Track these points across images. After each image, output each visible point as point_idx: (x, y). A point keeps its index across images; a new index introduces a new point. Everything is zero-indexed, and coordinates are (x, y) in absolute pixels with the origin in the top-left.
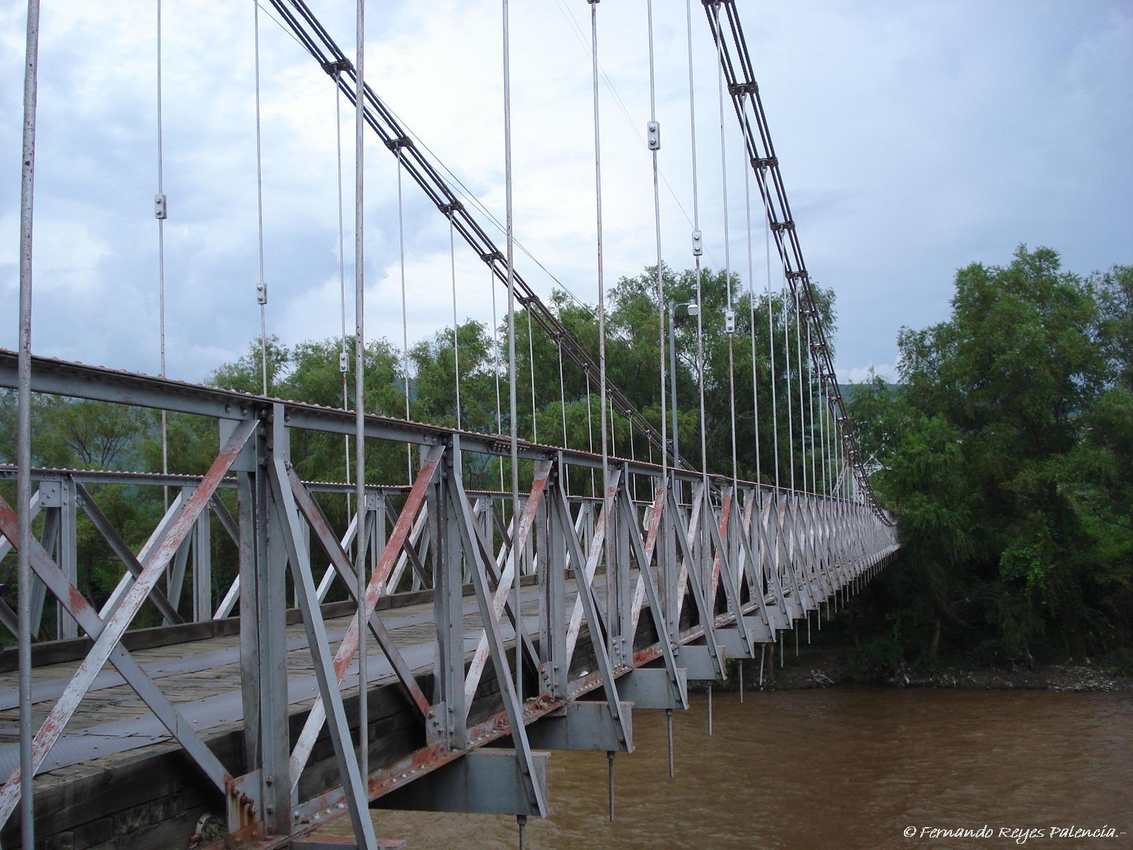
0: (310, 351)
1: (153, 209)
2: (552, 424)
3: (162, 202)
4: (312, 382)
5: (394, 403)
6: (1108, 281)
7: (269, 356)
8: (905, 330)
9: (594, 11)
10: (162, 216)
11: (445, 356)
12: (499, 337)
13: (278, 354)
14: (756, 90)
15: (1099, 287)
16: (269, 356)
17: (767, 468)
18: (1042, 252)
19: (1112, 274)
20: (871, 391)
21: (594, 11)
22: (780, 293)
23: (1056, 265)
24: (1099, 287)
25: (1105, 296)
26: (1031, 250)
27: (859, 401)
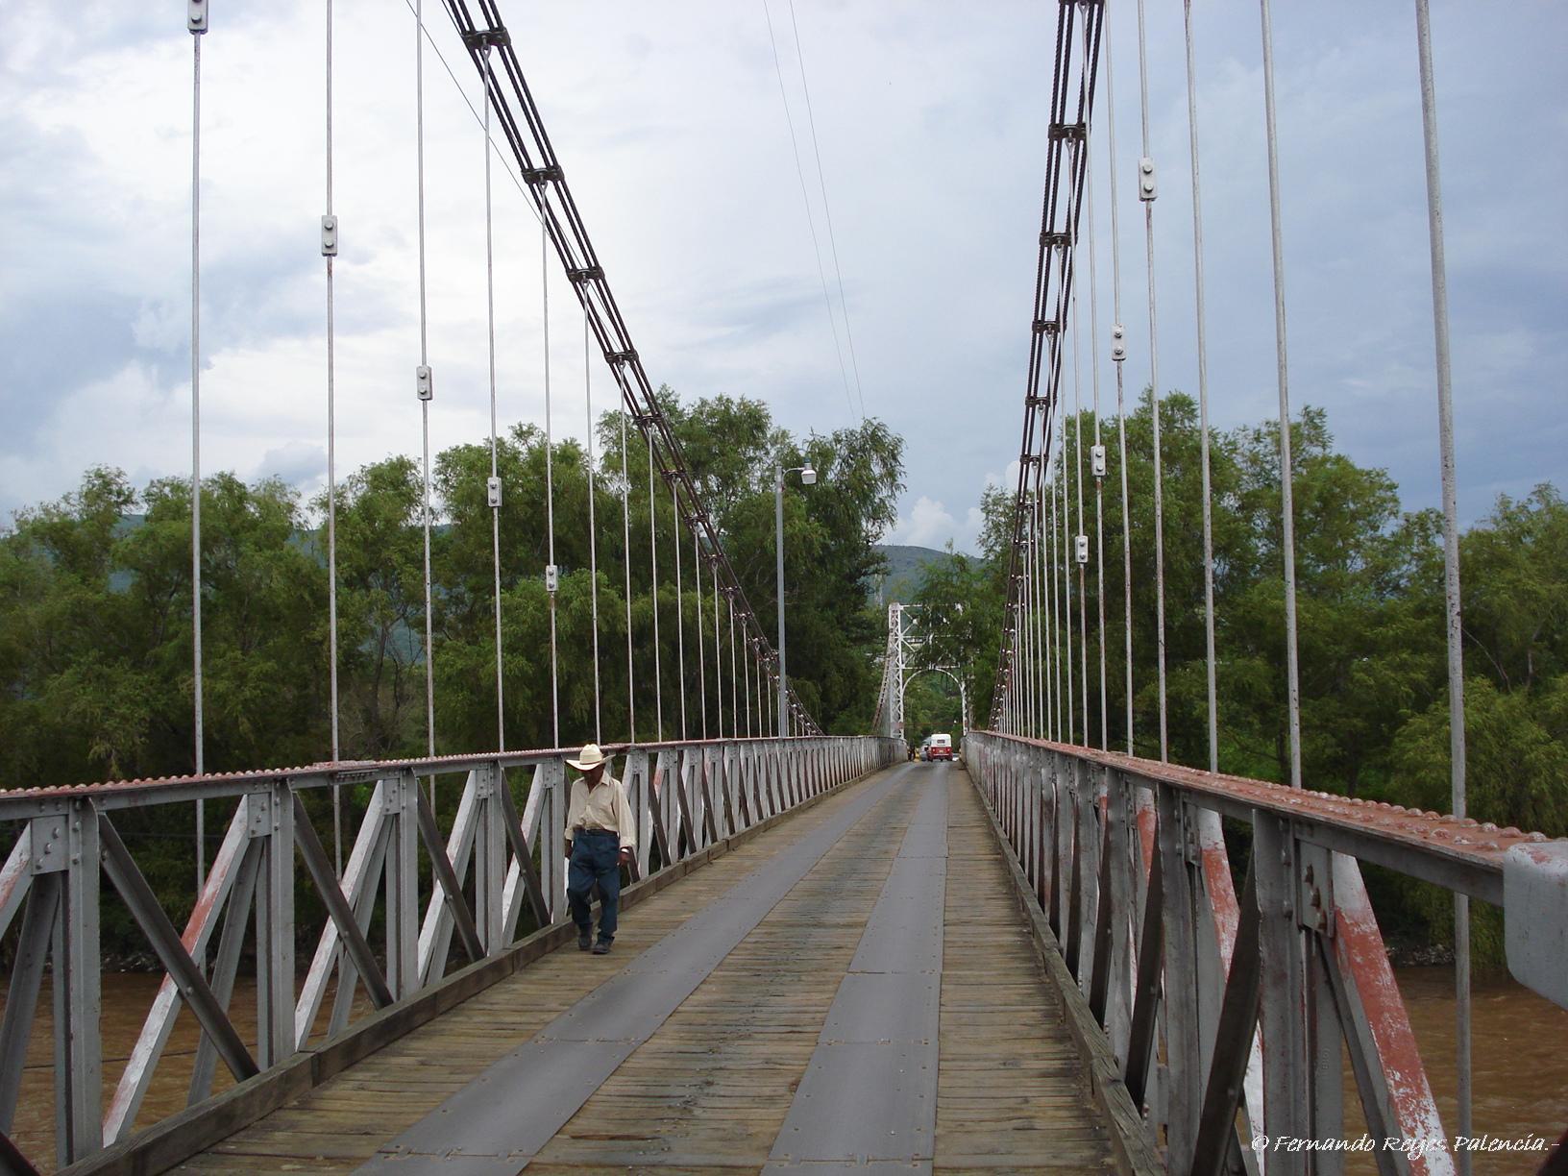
0: (167, 490)
1: (413, 387)
2: (525, 609)
3: (425, 377)
4: (170, 538)
5: (299, 570)
6: (1257, 439)
7: (104, 491)
8: (993, 493)
9: (1149, 211)
10: (425, 396)
11: (366, 507)
12: (433, 478)
13: (119, 494)
14: (1044, 234)
15: (1245, 445)
16: (104, 491)
17: (1055, 732)
18: (1185, 398)
19: (1264, 430)
20: (948, 574)
21: (1149, 211)
22: (831, 437)
23: (1191, 415)
24: (1245, 445)
25: (1254, 460)
26: (1161, 395)
27: (934, 586)
